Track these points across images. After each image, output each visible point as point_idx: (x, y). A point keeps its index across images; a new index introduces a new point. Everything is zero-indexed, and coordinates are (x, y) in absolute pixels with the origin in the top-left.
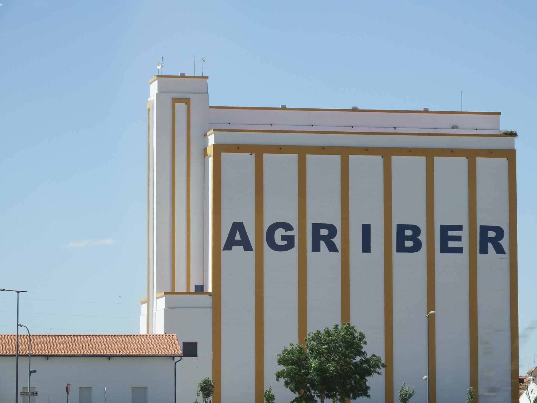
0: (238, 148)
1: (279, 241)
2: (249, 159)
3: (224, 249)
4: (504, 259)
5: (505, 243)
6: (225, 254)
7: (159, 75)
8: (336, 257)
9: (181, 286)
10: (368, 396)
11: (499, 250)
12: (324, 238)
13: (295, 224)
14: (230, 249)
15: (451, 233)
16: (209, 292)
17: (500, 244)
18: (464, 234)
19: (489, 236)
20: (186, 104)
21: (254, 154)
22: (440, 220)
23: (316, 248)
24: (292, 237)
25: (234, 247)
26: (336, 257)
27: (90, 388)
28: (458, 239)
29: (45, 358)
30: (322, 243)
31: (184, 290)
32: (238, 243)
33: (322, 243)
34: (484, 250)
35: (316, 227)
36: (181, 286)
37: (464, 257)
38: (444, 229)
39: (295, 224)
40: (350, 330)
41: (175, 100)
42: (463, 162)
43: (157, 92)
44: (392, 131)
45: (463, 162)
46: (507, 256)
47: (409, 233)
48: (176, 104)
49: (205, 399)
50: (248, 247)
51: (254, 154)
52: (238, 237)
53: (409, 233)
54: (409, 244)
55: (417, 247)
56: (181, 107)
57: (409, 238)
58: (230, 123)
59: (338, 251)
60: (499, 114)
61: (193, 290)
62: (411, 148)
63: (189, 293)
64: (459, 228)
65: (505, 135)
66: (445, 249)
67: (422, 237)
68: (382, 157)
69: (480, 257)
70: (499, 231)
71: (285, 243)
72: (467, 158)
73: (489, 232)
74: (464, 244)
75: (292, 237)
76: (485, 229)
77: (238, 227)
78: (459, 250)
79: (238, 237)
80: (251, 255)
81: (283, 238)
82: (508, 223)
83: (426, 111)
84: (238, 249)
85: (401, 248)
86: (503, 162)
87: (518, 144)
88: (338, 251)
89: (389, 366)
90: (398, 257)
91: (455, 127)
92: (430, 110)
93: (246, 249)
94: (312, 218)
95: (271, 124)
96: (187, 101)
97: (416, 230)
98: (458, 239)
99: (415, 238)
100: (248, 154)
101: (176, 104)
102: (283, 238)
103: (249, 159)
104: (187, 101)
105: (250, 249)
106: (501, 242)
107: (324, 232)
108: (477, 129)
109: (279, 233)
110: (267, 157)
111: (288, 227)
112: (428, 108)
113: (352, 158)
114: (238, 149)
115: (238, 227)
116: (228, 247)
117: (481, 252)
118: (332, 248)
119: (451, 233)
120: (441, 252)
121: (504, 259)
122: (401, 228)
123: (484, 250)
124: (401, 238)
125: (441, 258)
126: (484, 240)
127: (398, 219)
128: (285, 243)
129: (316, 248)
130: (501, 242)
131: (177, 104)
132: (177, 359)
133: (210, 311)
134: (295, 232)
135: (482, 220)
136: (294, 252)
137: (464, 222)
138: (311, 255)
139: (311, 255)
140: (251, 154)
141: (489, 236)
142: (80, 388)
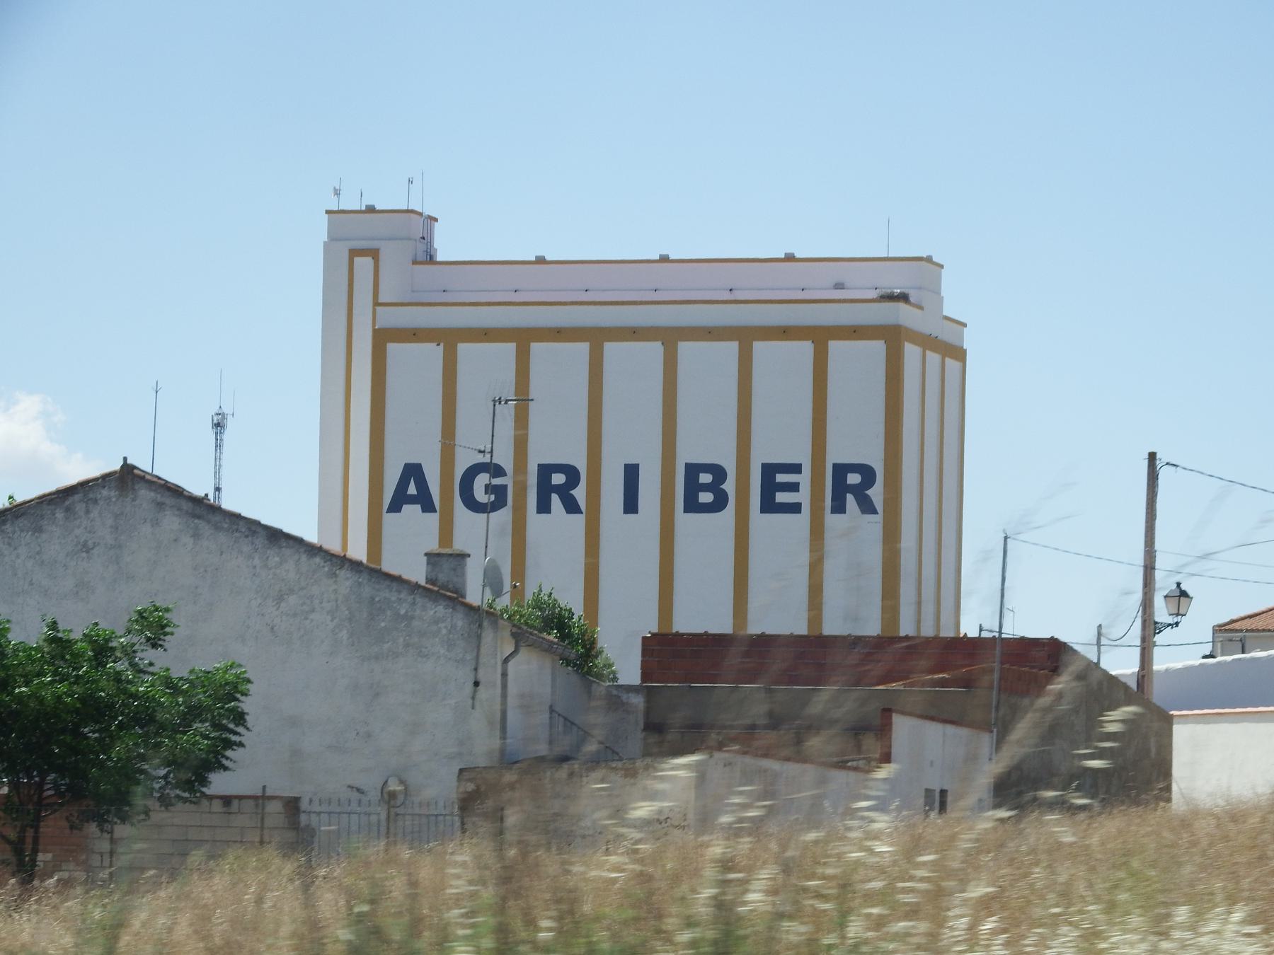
1: (481, 496)
2: (432, 353)
5: (876, 493)
6: (389, 519)
8: (579, 521)
12: (557, 489)
15: (781, 478)
17: (572, 495)
18: (804, 479)
21: (442, 344)
22: (761, 455)
28: (794, 487)
30: (555, 499)
32: (412, 500)
33: (555, 499)
34: (839, 508)
35: (546, 471)
37: (804, 518)
38: (769, 471)
41: (354, 253)
42: (654, 349)
44: (727, 296)
45: (654, 349)
46: (878, 519)
47: (705, 478)
50: (428, 507)
51: (442, 344)
52: (412, 490)
53: (705, 478)
54: (706, 498)
55: (719, 504)
57: (706, 488)
59: (582, 513)
62: (488, 329)
64: (796, 469)
66: (769, 506)
67: (729, 486)
68: (662, 344)
69: (833, 521)
74: (803, 497)
76: (841, 471)
77: (413, 471)
78: (795, 508)
79: (412, 490)
80: (433, 519)
81: (489, 489)
85: (692, 506)
90: (686, 522)
91: (839, 286)
95: (802, 287)
96: (374, 254)
97: (719, 473)
98: (794, 487)
99: (716, 487)
100: (433, 345)
104: (374, 254)
106: (869, 492)
109: (482, 480)
110: (536, 347)
111: (498, 471)
115: (413, 471)
116: (395, 507)
118: (571, 507)
119: (781, 478)
122: (693, 470)
123: (839, 508)
125: (760, 522)
126: (840, 490)
127: (688, 453)
129: (544, 507)
130: (869, 492)
135: (837, 453)
136: (503, 517)
140: (438, 345)
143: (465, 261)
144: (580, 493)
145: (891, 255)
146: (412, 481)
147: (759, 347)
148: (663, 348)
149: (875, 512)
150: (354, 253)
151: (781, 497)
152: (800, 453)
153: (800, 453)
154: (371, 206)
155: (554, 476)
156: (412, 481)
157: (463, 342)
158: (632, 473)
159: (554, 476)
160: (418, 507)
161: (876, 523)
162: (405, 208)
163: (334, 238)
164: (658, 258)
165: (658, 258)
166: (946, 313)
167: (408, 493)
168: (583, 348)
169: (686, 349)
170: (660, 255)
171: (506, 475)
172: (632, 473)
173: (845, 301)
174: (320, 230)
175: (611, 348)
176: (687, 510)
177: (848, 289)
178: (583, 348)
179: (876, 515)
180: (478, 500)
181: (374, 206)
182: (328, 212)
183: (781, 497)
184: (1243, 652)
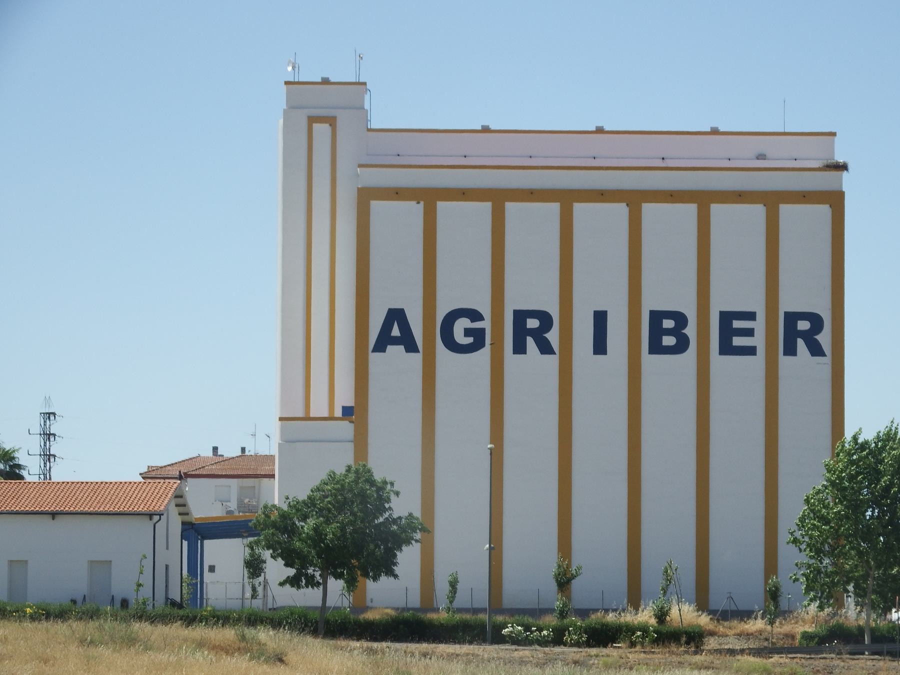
0: (397, 193)
1: (460, 338)
2: (414, 210)
3: (374, 351)
4: (823, 364)
5: (824, 338)
6: (375, 359)
7: (360, 81)
8: (552, 361)
9: (319, 408)
10: (396, 576)
11: (816, 350)
12: (533, 333)
13: (486, 311)
14: (383, 350)
15: (737, 324)
16: (335, 416)
17: (817, 341)
18: (759, 325)
19: (799, 328)
20: (330, 125)
21: (422, 203)
22: (719, 303)
23: (520, 348)
24: (482, 331)
25: (389, 348)
26: (552, 361)
27: (26, 562)
28: (750, 333)
29: (50, 517)
30: (800, 343)
31: (326, 414)
32: (395, 341)
33: (800, 343)
34: (790, 350)
35: (520, 316)
36: (319, 408)
37: (757, 362)
38: (726, 318)
39: (486, 311)
40: (362, 474)
41: (313, 120)
42: (620, 210)
43: (285, 108)
44: (659, 163)
45: (620, 210)
46: (827, 360)
47: (668, 324)
48: (314, 125)
49: (251, 580)
50: (411, 347)
51: (422, 203)
52: (396, 332)
53: (668, 324)
54: (669, 341)
55: (682, 346)
56: (322, 130)
57: (669, 332)
58: (399, 154)
59: (554, 353)
60: (833, 134)
61: (338, 413)
62: (674, 191)
63: (331, 418)
64: (751, 316)
65: (828, 169)
66: (727, 349)
67: (691, 331)
68: (830, 206)
69: (785, 361)
70: (816, 321)
71: (470, 340)
72: (765, 205)
73: (799, 321)
74: (758, 341)
75: (482, 331)
76: (792, 318)
77: (396, 316)
78: (750, 351)
79: (396, 332)
80: (416, 359)
81: (468, 332)
82: (830, 307)
83: (715, 132)
84: (395, 351)
85: (656, 348)
86: (824, 211)
87: (848, 182)
88: (554, 353)
89: (427, 530)
90: (651, 362)
91: (761, 157)
92: (722, 129)
93: (408, 350)
94: (513, 302)
95: (795, 158)
96: (331, 121)
97: (680, 319)
98: (750, 333)
99: (678, 331)
100: (413, 203)
101: (314, 125)
102: (468, 332)
103: (414, 210)
104: (331, 121)
105: (416, 350)
106: (547, 335)
107: (533, 323)
108: (796, 160)
109: (461, 325)
110: (442, 206)
111: (475, 315)
112: (603, 127)
113: (442, 206)
114: (670, 197)
115: (396, 316)
116: (380, 347)
117: (786, 353)
118: (545, 348)
119: (737, 324)
120: (784, 355)
121: (823, 364)
122: (657, 317)
123: (790, 350)
124: (656, 332)
125: (719, 363)
127: (651, 302)
128: (470, 340)
129: (520, 348)
130: (547, 335)
131: (316, 126)
132: (156, 518)
133: (350, 447)
134: (486, 324)
135: (789, 303)
136: (484, 355)
137: (758, 305)
138: (510, 357)
139: (510, 357)
140: (418, 203)
141: (799, 328)
142: (11, 562)
143: (645, 131)
144: (553, 336)
145: (786, 131)
146: (396, 322)
147: (443, 207)
148: (628, 208)
149: (553, 352)
150: (313, 120)
151: (738, 341)
152: (756, 303)
153: (756, 303)
154: (325, 78)
155: (664, 321)
156: (396, 322)
157: (375, 200)
158: (600, 319)
159: (664, 321)
160: (402, 348)
161: (825, 364)
162: (353, 79)
163: (292, 107)
164: (595, 129)
165: (595, 129)
166: (374, 125)
167: (400, 335)
168: (554, 208)
169: (649, 210)
170: (596, 127)
171: (484, 320)
172: (600, 319)
173: (793, 169)
174: (279, 99)
175: (579, 209)
176: (785, 354)
177: (769, 159)
178: (554, 208)
179: (825, 357)
180: (460, 343)
181: (328, 78)
182: (286, 83)
183: (738, 341)
184: (273, 476)
